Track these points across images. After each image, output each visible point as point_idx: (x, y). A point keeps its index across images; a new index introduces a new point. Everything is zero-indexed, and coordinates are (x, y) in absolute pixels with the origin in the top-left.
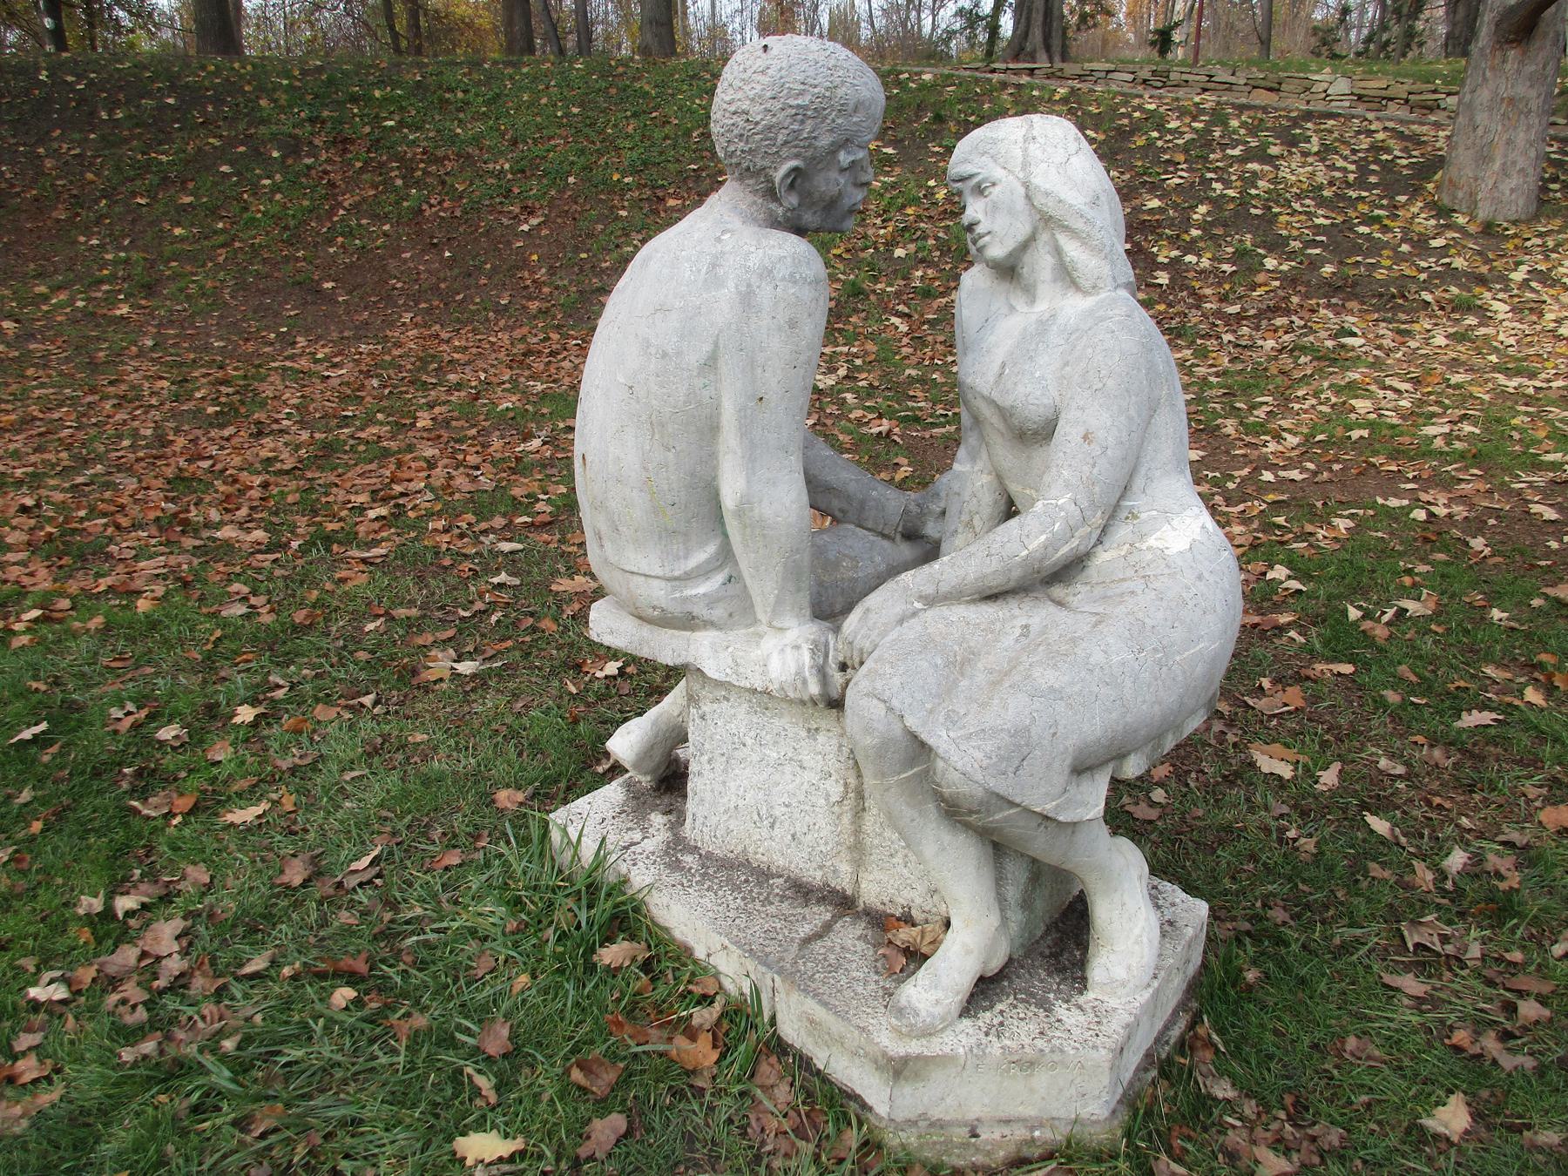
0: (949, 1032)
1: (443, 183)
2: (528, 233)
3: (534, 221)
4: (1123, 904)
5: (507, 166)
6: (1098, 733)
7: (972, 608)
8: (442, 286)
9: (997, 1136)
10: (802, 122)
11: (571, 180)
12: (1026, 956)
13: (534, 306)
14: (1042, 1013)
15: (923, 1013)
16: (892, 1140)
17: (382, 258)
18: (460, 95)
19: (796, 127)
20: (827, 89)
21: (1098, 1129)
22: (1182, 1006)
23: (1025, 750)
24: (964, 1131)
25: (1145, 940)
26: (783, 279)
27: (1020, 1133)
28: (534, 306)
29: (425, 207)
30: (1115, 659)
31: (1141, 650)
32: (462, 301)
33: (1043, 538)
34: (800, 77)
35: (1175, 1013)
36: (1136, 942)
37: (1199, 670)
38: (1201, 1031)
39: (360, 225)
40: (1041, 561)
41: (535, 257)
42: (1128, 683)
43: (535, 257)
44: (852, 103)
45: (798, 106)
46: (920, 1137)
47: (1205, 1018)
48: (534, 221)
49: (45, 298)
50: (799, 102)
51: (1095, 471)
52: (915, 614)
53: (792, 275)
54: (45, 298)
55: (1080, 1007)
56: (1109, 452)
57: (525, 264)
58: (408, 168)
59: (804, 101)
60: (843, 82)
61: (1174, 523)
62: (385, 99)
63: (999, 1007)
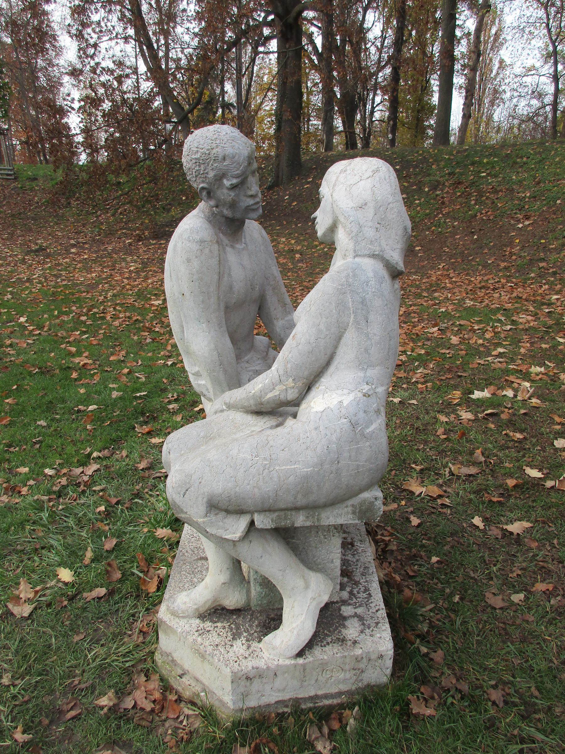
0: (185, 620)
1: (493, 203)
2: (520, 229)
3: (527, 223)
4: (293, 607)
5: (528, 195)
6: (220, 491)
7: (245, 416)
8: (466, 252)
9: (188, 683)
10: (200, 166)
11: (558, 202)
12: (260, 612)
13: (503, 265)
14: (230, 638)
15: (176, 604)
16: (157, 657)
17: (446, 237)
18: (525, 159)
19: (197, 168)
20: (208, 150)
21: (223, 710)
22: (349, 693)
23: (188, 486)
24: (180, 672)
25: (295, 632)
26: (185, 239)
27: (198, 688)
28: (503, 265)
29: (479, 214)
30: (241, 455)
31: (257, 456)
32: (471, 260)
33: (260, 385)
34: (196, 145)
35: (340, 694)
36: (290, 631)
37: (291, 479)
38: (347, 712)
39: (445, 222)
40: (260, 398)
41: (517, 241)
42: (242, 470)
43: (517, 241)
44: (220, 157)
45: (196, 159)
46: (164, 662)
47: (357, 708)
48: (527, 223)
49: (317, 246)
50: (196, 157)
51: (290, 355)
52: (222, 411)
53: (189, 237)
54: (317, 246)
55: (249, 647)
56: (300, 347)
57: (511, 244)
58: (480, 194)
59: (198, 156)
60: (217, 147)
61: (326, 395)
62: (487, 163)
63: (219, 624)
